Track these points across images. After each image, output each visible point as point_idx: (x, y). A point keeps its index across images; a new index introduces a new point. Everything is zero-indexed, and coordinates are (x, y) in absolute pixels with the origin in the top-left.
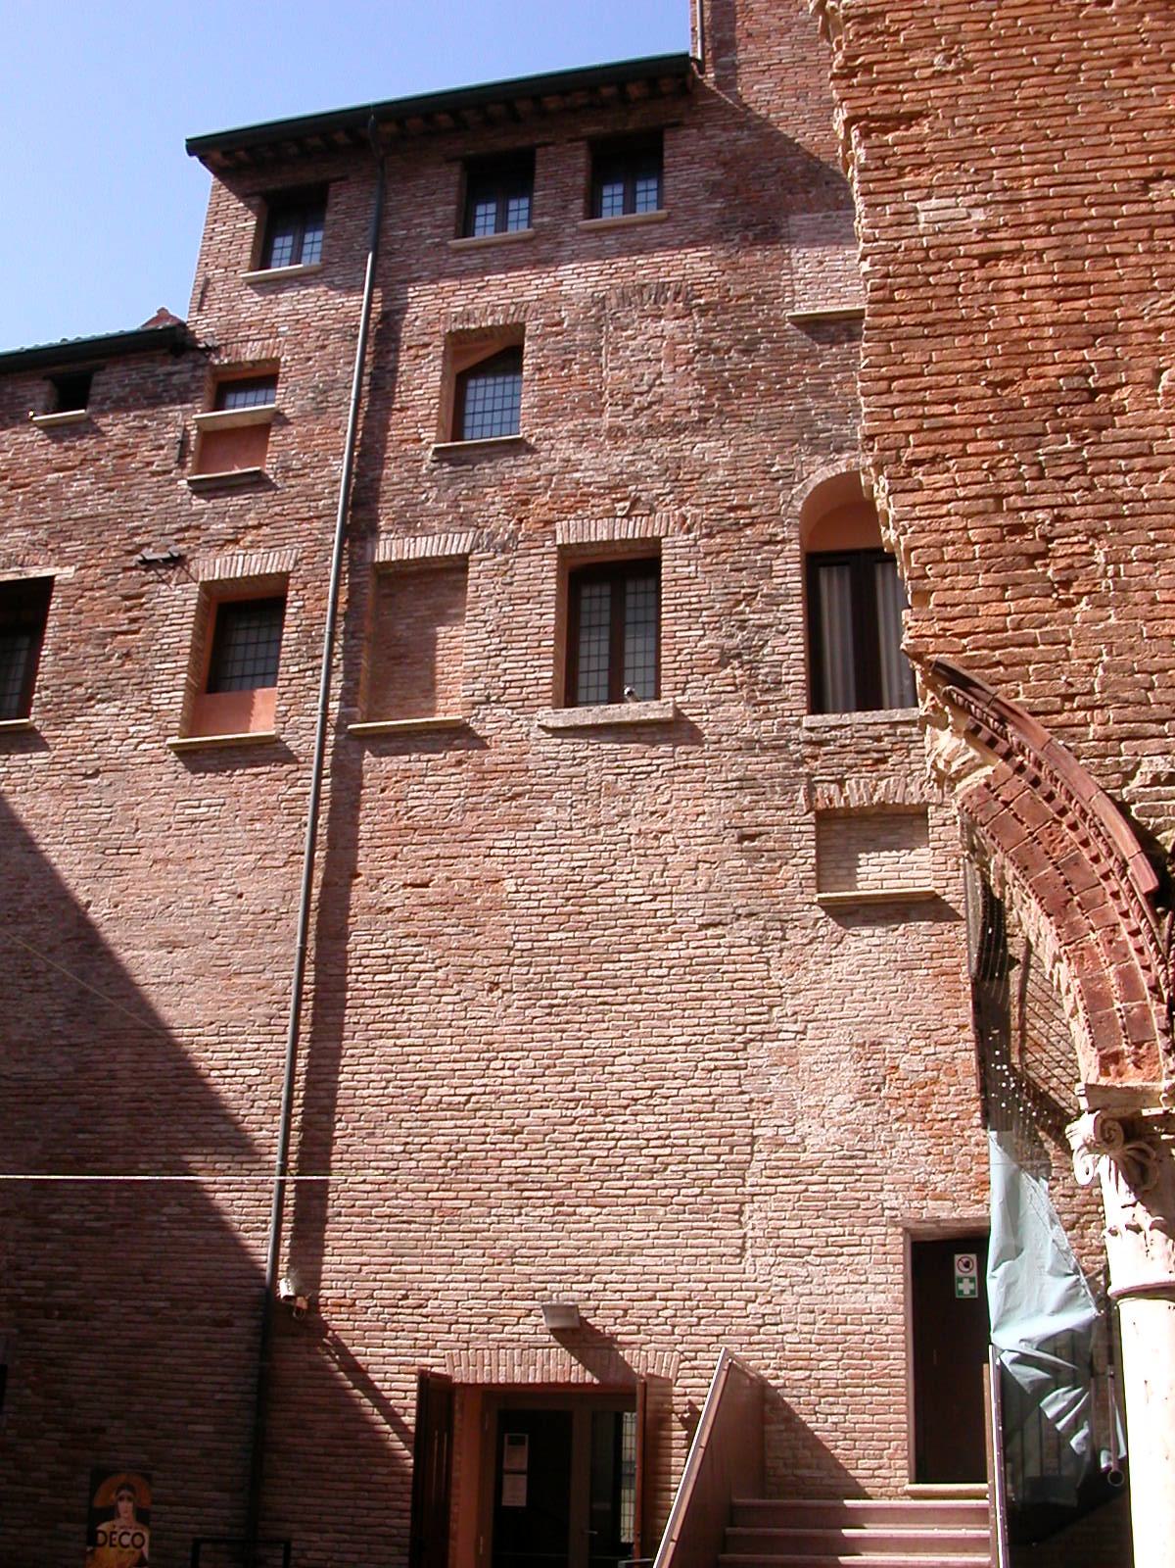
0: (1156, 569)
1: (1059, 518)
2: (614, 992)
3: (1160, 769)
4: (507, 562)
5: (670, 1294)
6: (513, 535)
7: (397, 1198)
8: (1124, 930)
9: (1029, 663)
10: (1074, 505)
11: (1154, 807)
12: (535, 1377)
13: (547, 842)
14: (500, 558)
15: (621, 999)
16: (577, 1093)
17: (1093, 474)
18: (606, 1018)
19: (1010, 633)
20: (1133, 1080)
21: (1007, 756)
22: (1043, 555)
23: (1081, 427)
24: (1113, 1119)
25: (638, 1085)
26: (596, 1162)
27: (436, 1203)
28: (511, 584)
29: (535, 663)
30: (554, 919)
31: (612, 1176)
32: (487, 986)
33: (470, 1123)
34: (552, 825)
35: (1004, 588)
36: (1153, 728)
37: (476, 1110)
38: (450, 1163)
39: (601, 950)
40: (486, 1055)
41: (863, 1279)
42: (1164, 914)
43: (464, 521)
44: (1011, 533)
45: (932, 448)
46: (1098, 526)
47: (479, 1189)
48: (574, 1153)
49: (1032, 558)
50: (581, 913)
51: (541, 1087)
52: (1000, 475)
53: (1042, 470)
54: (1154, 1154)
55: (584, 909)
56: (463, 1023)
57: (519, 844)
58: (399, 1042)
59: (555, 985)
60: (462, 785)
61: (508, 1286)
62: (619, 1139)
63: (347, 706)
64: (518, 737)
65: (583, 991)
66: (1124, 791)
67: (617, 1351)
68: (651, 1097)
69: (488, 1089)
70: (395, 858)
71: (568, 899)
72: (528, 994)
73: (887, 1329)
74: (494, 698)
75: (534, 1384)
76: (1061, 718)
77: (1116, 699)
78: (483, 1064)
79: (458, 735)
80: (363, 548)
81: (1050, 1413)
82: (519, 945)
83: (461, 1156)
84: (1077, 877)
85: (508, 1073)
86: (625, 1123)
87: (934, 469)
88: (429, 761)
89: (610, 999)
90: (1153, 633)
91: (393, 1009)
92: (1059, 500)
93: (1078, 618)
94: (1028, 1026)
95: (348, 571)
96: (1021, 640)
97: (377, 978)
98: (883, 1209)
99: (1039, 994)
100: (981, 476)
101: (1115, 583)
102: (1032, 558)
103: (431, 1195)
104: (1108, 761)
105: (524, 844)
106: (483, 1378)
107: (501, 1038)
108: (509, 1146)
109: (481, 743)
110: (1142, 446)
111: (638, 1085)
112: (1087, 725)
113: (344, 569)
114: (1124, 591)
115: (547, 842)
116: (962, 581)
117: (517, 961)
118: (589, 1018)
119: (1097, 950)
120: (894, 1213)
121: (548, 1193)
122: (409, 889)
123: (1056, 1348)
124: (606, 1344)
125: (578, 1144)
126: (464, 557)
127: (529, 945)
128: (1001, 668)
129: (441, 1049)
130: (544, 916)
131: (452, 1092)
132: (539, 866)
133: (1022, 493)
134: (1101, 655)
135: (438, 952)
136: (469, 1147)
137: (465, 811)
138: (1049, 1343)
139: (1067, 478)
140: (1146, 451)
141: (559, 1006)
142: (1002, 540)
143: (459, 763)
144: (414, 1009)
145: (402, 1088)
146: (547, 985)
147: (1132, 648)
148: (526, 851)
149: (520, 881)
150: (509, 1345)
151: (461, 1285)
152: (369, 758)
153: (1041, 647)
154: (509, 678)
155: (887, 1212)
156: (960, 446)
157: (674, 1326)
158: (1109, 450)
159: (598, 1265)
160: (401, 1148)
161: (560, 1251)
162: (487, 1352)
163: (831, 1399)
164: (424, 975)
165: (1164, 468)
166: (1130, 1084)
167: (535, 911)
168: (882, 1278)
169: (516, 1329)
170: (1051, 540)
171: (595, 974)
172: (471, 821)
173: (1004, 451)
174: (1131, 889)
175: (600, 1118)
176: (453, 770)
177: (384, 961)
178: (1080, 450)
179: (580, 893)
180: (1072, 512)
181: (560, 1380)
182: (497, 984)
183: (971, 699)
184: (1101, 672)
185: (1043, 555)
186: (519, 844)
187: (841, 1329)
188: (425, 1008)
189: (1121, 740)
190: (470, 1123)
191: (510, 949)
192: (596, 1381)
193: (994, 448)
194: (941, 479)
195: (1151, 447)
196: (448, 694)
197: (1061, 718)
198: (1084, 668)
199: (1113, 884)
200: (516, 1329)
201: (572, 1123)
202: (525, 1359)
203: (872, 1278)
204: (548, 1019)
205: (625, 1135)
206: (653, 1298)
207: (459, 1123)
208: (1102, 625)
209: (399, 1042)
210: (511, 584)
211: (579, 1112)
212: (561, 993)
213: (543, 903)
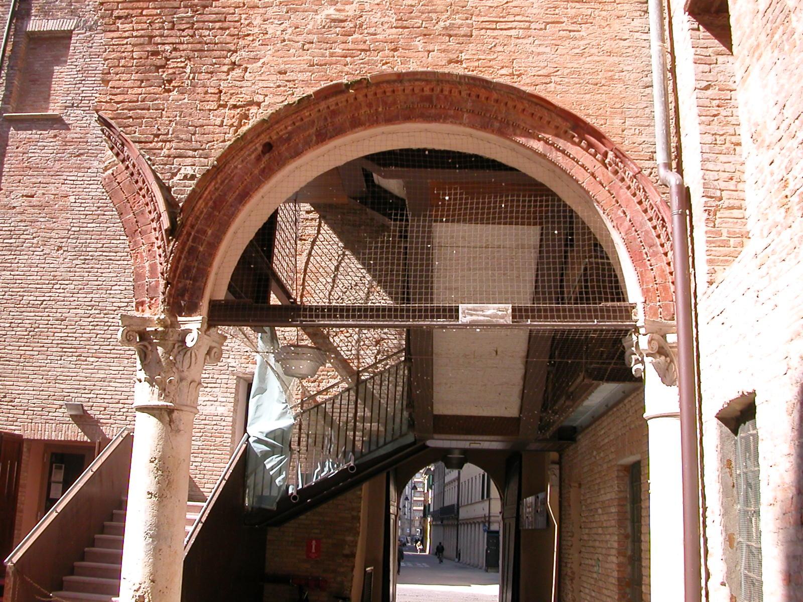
0: (212, 77)
1: (175, 49)
2: (115, 254)
3: (189, 172)
4: (91, 36)
5: (126, 401)
6: (96, 22)
7: (5, 349)
8: (156, 245)
9: (144, 118)
10: (183, 43)
11: (181, 190)
12: (61, 437)
13: (92, 179)
14: (88, 34)
15: (118, 258)
16: (93, 303)
17: (196, 29)
18: (110, 267)
19: (139, 103)
20: (147, 314)
21: (123, 161)
22: (163, 67)
23: (196, 6)
24: (133, 331)
25: (122, 300)
26: (98, 336)
27: (22, 352)
28: (91, 47)
29: (98, 88)
30: (91, 217)
31: (105, 343)
32: (56, 248)
33: (41, 314)
34: (95, 170)
35: (142, 81)
36: (191, 153)
37: (45, 308)
38: (31, 333)
39: (112, 233)
40: (53, 282)
41: (215, 399)
42: (172, 240)
43: (73, 13)
44: (152, 55)
45: (127, 11)
46: (191, 54)
47: (43, 347)
48: (88, 331)
49: (158, 68)
50: (104, 215)
51: (76, 299)
52: (154, 27)
53: (174, 25)
54: (150, 348)
55: (106, 213)
56: (43, 266)
57: (79, 179)
58: (12, 273)
59: (88, 249)
60: (55, 147)
61: (52, 394)
62: (110, 326)
63: (5, 104)
64: (85, 125)
65: (101, 253)
66: (171, 181)
67: (99, 427)
68: (127, 306)
69: (52, 298)
70: (19, 182)
71: (99, 207)
72: (74, 253)
73: (224, 424)
74: (75, 105)
75: (61, 441)
76: (151, 145)
77: (177, 137)
78: (51, 286)
79: (57, 122)
80: (22, 23)
81: (268, 466)
82: (73, 229)
83: (36, 330)
84: (142, 220)
85: (62, 291)
86: (113, 318)
87: (126, 21)
88: (41, 134)
89: (113, 258)
90: (202, 108)
91: (11, 257)
92: (177, 41)
93: (171, 99)
94: (306, 284)
95: (14, 35)
96: (143, 107)
97: (5, 241)
98: (228, 367)
99: (314, 269)
100: (145, 26)
101: (191, 82)
102: (158, 68)
103: (21, 348)
104: (167, 167)
105: (81, 179)
106: (38, 437)
107: (60, 274)
108: (59, 327)
109: (67, 127)
110: (221, 17)
111: (122, 300)
112: (162, 149)
113: (12, 33)
114: (194, 87)
115: (92, 179)
116: (125, 77)
117: (72, 237)
118: (102, 267)
119: (144, 254)
120: (233, 369)
121: (75, 350)
122: (25, 198)
123: (275, 437)
124: (95, 423)
125: (91, 327)
126: (71, 31)
127: (78, 229)
128: (131, 120)
129: (31, 278)
130: (86, 215)
131: (35, 299)
132: (87, 190)
133: (161, 36)
134: (176, 116)
135: (35, 230)
136: (41, 326)
137: (55, 161)
138: (271, 434)
139: (183, 30)
140: (223, 19)
141: (89, 259)
142: (147, 58)
143: (55, 136)
144: (21, 257)
145: (12, 295)
146: (84, 249)
147: (191, 114)
148: (82, 182)
149: (77, 197)
150: (51, 422)
151: (31, 392)
152: (12, 131)
153: (151, 111)
154: (84, 95)
155: (230, 369)
156: (140, 11)
157: (127, 416)
158: (206, 18)
159: (94, 385)
160: (9, 325)
161: (78, 378)
162: (40, 425)
163: (195, 455)
164: (27, 241)
165: (228, 28)
166: (145, 316)
167: (82, 213)
168: (224, 399)
169: (54, 414)
170: (168, 60)
171: (107, 245)
172: (58, 165)
173: (160, 14)
174: (160, 227)
175: (102, 315)
176: (52, 140)
177: (9, 233)
178: (193, 17)
179: (105, 205)
180: (181, 47)
181: (73, 439)
182: (61, 247)
183: (111, 133)
184: (174, 125)
185: (163, 67)
186: (79, 179)
187: (203, 422)
188: (26, 257)
189: (175, 157)
190: (41, 314)
191: (69, 230)
192: (89, 441)
193: (155, 13)
194: (128, 27)
195: (226, 18)
196: (56, 101)
197: (151, 145)
198: (167, 122)
199: (154, 225)
200: (54, 414)
201: (89, 317)
202: (58, 428)
203: (220, 399)
204: (83, 266)
205: (113, 324)
206: (118, 403)
207: (37, 314)
208: (180, 102)
209: (12, 273)
210: (91, 47)
211: (93, 311)
212: (90, 254)
213: (87, 209)
